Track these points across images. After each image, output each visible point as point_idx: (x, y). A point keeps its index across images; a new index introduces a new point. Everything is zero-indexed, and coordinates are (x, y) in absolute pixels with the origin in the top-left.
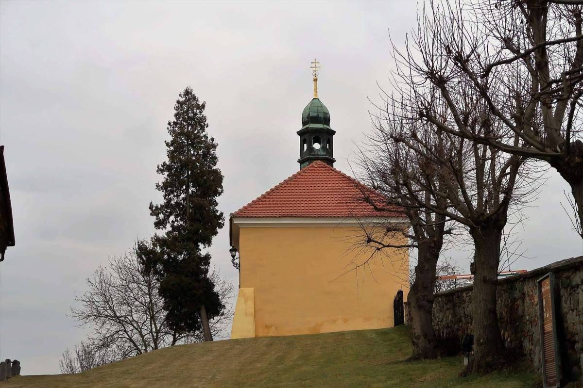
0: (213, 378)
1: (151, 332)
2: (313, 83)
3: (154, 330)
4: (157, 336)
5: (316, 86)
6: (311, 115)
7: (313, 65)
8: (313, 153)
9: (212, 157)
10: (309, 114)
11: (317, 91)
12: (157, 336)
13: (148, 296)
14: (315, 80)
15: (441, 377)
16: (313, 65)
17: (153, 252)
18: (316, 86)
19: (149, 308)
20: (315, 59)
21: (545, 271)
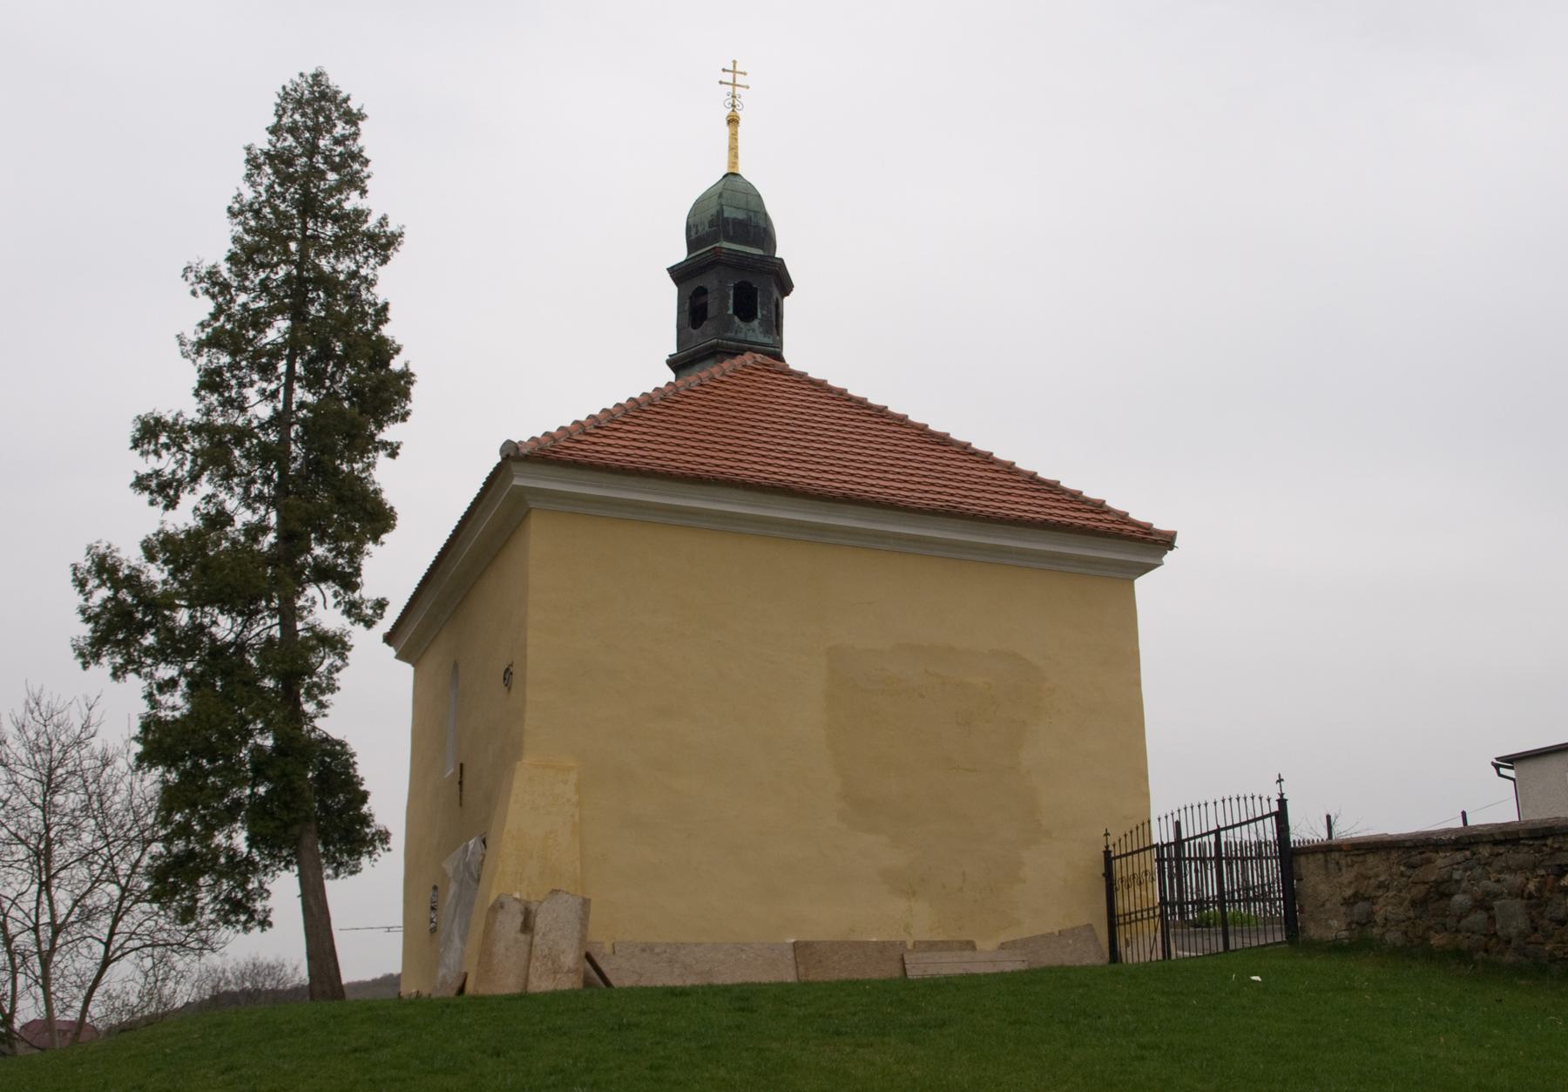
0: (72, 891)
1: (35, 929)
2: (725, 130)
3: (45, 919)
4: (53, 941)
5: (734, 137)
6: (726, 214)
7: (728, 77)
8: (729, 335)
9: (328, 393)
10: (720, 212)
11: (736, 156)
12: (53, 941)
13: (861, 1050)
14: (733, 121)
15: (819, 1082)
16: (728, 77)
17: (133, 581)
18: (734, 137)
19: (37, 853)
20: (735, 62)
21: (203, 824)
